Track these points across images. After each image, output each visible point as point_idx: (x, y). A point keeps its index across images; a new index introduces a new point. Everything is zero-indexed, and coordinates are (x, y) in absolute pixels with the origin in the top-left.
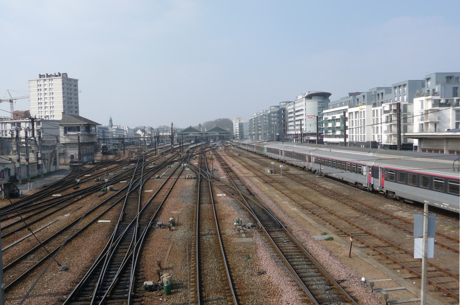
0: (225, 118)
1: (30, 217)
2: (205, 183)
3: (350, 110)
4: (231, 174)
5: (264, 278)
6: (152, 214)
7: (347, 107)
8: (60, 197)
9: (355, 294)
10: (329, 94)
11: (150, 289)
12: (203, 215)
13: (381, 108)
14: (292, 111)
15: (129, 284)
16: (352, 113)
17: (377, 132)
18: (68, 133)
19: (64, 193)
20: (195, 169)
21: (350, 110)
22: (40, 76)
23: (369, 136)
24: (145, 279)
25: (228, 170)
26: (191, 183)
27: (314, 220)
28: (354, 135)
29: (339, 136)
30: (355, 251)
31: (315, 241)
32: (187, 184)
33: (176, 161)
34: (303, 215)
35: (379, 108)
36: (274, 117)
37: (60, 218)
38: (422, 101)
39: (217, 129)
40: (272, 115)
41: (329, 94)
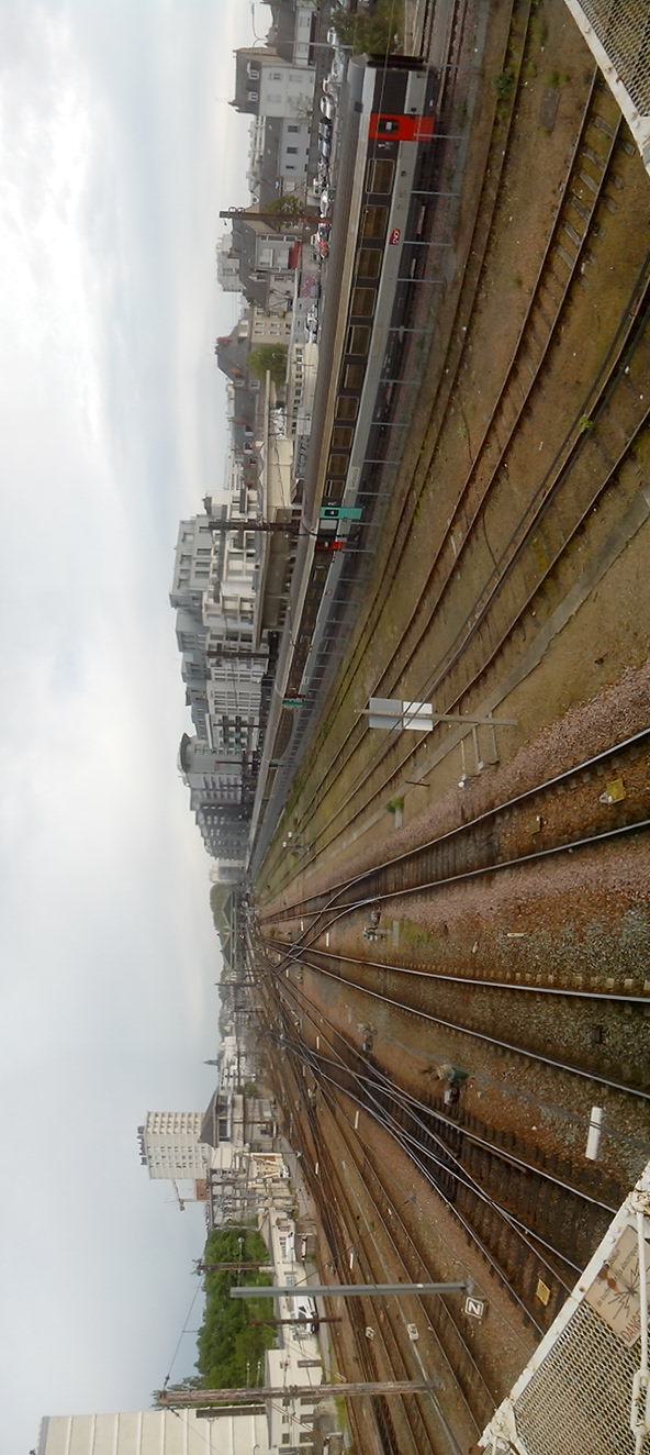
0: (209, 896)
1: (336, 1191)
2: (304, 952)
3: (212, 711)
4: (297, 910)
5: (452, 926)
6: (350, 1051)
7: (207, 716)
8: (356, 1253)
9: (468, 394)
10: (185, 735)
11: (455, 1097)
12: (355, 974)
13: (213, 669)
14: (205, 793)
15: (445, 1123)
16: (216, 709)
17: (249, 676)
18: (229, 1135)
19: (349, 1244)
20: (288, 963)
21: (212, 711)
22: (144, 1161)
23: (255, 691)
24: (442, 1100)
25: (290, 913)
26: (309, 976)
27: (372, 814)
28: (250, 712)
29: (250, 732)
30: (419, 775)
31: (404, 825)
32: (308, 982)
33: (274, 985)
34: (365, 827)
35: (214, 671)
36: (213, 820)
37: (346, 1174)
38: (208, 615)
39: (227, 910)
40: (209, 822)
41: (185, 735)
